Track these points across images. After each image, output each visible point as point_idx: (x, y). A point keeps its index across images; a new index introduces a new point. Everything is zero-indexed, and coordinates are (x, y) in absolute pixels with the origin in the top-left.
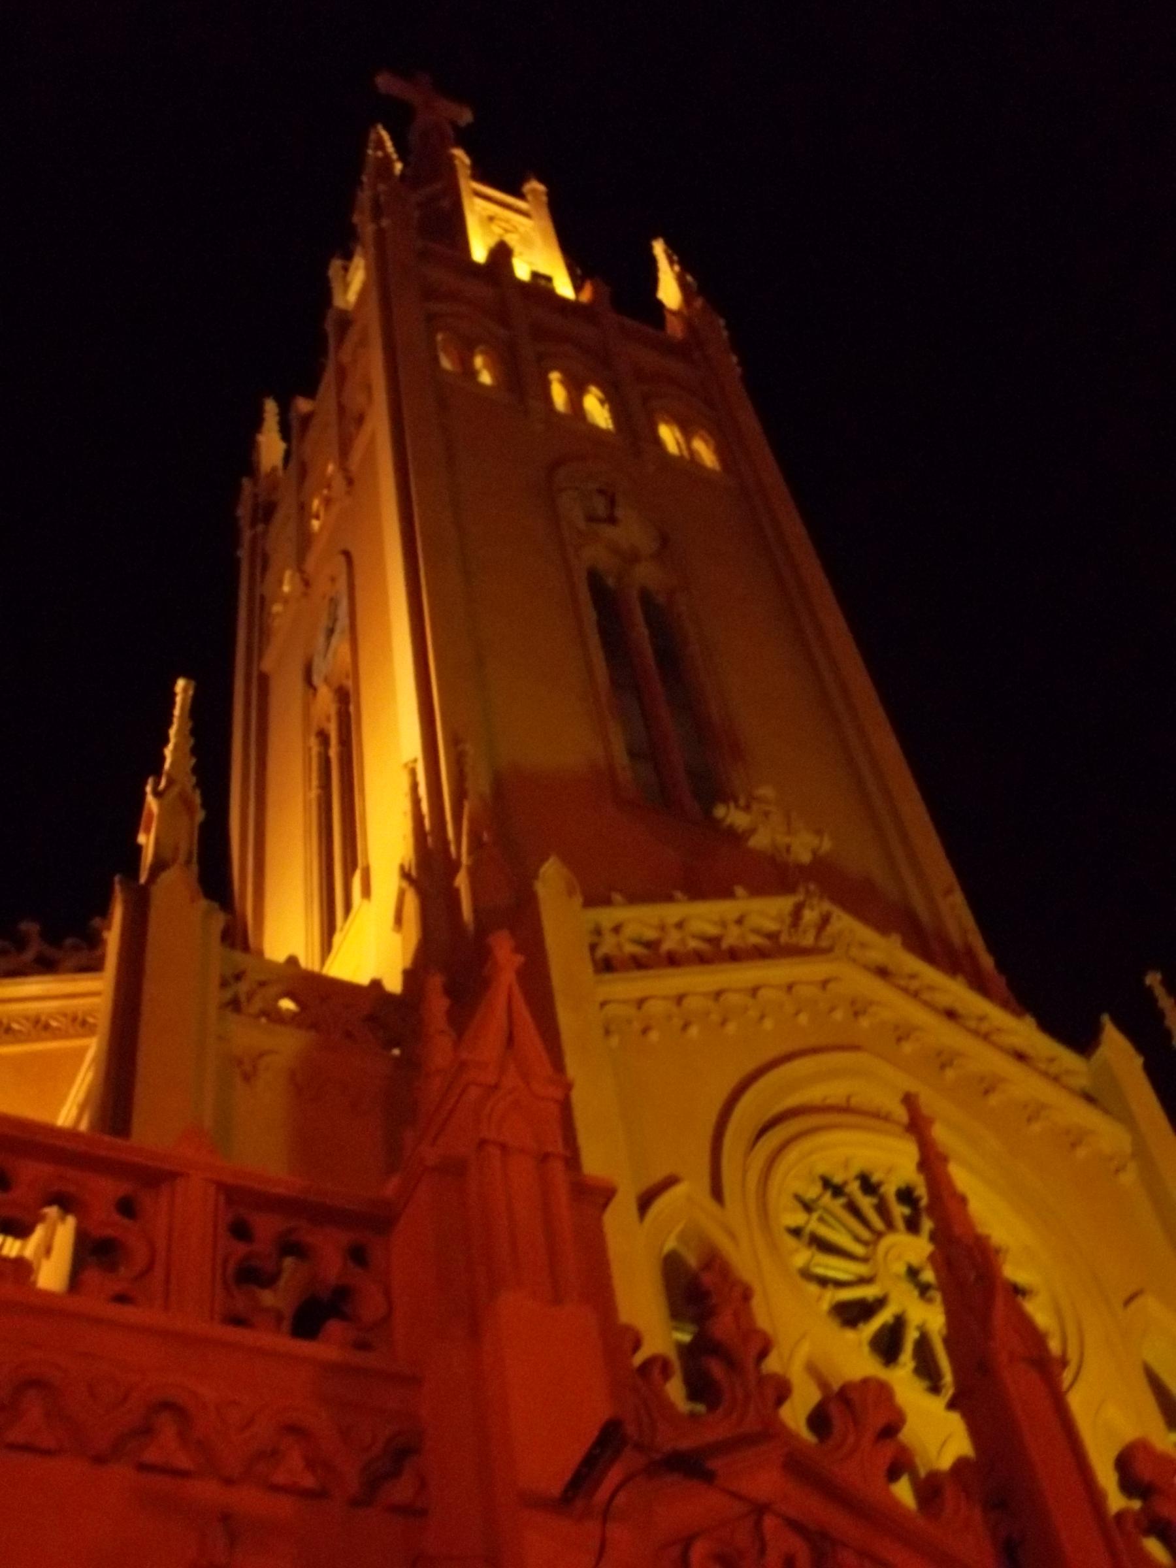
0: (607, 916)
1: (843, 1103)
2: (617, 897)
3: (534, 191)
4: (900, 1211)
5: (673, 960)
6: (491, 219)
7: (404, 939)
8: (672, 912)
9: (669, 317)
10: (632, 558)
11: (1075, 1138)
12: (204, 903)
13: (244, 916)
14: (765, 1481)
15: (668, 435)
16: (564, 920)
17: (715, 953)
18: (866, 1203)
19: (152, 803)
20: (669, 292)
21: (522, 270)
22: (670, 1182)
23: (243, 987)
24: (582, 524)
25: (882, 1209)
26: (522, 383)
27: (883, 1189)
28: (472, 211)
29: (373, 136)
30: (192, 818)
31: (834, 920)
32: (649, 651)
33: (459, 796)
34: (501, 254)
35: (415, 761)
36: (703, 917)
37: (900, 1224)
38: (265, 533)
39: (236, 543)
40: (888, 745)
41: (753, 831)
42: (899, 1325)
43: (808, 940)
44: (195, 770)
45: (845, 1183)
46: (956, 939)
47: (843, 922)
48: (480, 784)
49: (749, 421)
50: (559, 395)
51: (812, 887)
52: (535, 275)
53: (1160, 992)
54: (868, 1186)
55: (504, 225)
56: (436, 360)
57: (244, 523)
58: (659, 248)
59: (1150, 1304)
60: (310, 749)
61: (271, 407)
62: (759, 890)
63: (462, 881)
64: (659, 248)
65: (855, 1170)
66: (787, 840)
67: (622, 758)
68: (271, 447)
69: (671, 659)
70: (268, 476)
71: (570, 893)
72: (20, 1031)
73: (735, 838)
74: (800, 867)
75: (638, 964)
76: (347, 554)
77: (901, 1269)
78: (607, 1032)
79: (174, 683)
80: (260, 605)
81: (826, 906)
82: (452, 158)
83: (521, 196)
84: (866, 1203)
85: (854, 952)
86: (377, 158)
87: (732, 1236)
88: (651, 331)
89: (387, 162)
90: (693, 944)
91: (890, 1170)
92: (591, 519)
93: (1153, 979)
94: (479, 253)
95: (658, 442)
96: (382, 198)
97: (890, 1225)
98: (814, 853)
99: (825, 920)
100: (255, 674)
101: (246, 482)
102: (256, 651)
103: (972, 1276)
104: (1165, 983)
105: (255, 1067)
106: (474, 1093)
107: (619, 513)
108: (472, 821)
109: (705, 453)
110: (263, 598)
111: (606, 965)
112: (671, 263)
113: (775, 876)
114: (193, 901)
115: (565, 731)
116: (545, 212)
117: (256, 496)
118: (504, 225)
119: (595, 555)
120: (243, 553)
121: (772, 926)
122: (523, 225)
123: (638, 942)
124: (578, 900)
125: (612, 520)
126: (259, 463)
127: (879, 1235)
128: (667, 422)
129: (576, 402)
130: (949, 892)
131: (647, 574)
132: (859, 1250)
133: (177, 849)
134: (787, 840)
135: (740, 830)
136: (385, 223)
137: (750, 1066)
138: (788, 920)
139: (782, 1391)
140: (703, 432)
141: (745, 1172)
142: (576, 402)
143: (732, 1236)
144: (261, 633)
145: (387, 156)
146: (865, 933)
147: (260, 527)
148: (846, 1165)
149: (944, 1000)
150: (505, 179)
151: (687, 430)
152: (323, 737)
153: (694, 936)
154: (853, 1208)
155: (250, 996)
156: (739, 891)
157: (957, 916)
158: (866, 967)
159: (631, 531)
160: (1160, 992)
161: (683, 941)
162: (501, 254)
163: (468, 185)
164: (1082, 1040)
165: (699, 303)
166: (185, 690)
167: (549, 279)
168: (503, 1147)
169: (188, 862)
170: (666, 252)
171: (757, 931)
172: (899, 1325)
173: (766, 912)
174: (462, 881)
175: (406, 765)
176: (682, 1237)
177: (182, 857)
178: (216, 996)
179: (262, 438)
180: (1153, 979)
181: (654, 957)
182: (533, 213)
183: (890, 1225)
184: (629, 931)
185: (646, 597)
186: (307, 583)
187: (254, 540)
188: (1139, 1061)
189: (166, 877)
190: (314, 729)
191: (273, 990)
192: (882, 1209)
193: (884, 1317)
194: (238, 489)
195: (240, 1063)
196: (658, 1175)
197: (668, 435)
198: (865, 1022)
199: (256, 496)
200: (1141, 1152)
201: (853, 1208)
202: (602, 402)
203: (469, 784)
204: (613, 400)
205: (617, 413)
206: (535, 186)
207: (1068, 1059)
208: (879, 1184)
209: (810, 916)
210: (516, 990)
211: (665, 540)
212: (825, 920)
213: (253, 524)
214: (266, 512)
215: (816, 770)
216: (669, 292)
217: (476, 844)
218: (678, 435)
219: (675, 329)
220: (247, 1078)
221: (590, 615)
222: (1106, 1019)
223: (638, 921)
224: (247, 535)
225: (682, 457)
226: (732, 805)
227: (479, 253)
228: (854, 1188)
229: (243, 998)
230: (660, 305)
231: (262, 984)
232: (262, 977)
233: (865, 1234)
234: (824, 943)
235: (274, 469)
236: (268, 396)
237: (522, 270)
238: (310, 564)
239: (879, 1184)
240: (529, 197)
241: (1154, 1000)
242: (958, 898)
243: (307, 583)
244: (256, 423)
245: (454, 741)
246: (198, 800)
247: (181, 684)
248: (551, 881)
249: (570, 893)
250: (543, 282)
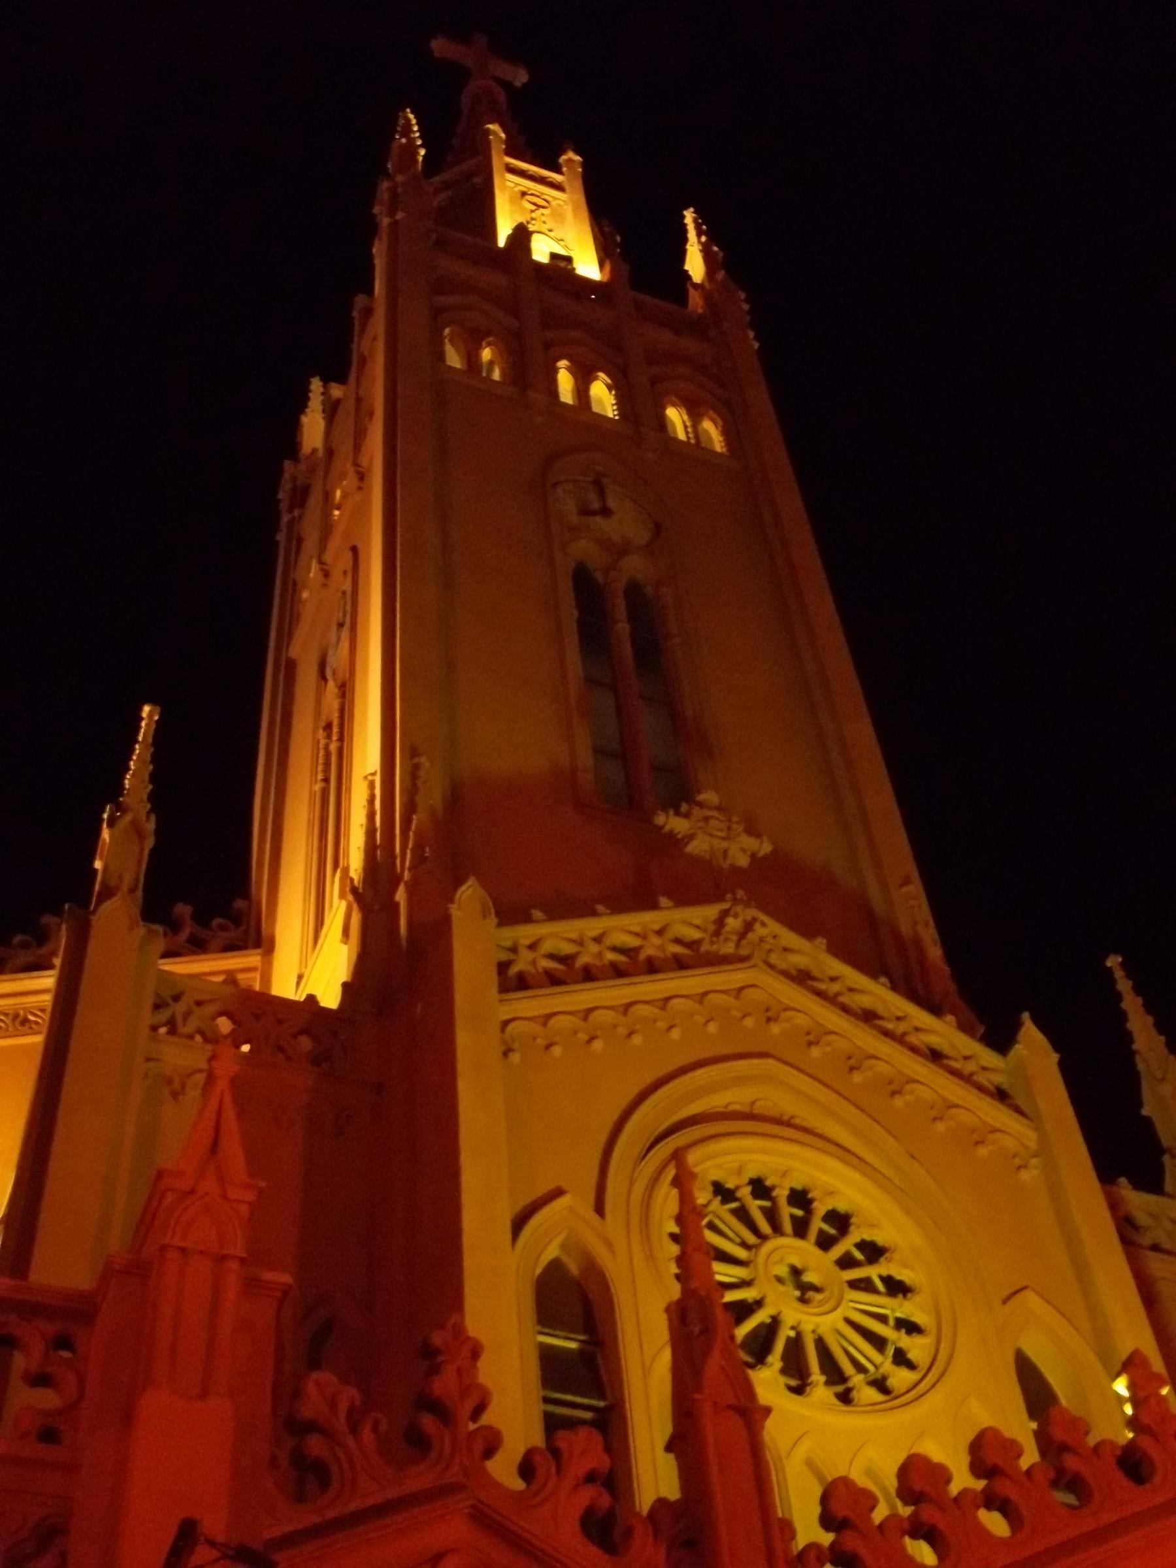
0: (525, 933)
1: (746, 1109)
2: (537, 914)
3: (570, 160)
4: (787, 1212)
5: (589, 975)
6: (524, 194)
7: (349, 950)
8: (590, 926)
9: (692, 291)
10: (623, 550)
11: (980, 1136)
12: (141, 930)
13: (259, 903)
14: (451, 1529)
15: (675, 416)
16: (475, 938)
17: (632, 965)
18: (755, 1206)
19: (106, 834)
20: (695, 265)
21: (541, 250)
22: (558, 1193)
23: (180, 1008)
24: (575, 519)
25: (772, 1215)
26: (530, 375)
27: (774, 1194)
28: (504, 187)
29: (402, 121)
30: (141, 844)
31: (757, 926)
32: (628, 649)
33: (410, 808)
34: (522, 235)
35: (374, 774)
36: (623, 928)
37: (787, 1226)
38: (300, 517)
39: (275, 527)
40: (862, 734)
41: (690, 837)
42: (773, 1326)
43: (729, 948)
44: (152, 797)
45: (738, 1188)
46: (905, 928)
47: (770, 928)
48: (433, 795)
49: (760, 398)
50: (565, 382)
51: (740, 893)
52: (554, 256)
53: (1119, 974)
54: (760, 1188)
55: (535, 200)
56: (441, 356)
57: (283, 506)
58: (689, 216)
59: (1032, 1301)
60: (318, 741)
61: (316, 385)
62: (684, 899)
63: (401, 895)
64: (689, 216)
65: (752, 1173)
66: (725, 845)
67: (585, 758)
68: (313, 428)
69: (650, 650)
70: (308, 457)
71: (485, 916)
72: (37, 1023)
73: (674, 842)
74: (735, 870)
75: (553, 980)
76: (354, 550)
77: (783, 1271)
78: (775, 937)
79: (140, 710)
80: (292, 589)
81: (752, 913)
82: (488, 132)
83: (557, 169)
84: (755, 1206)
85: (774, 958)
86: (402, 145)
87: (609, 1245)
88: (676, 307)
89: (412, 150)
90: (611, 956)
91: (784, 1174)
92: (585, 512)
93: (1113, 961)
94: (503, 232)
95: (662, 424)
96: (400, 190)
97: (777, 1229)
98: (753, 856)
99: (749, 926)
100: (284, 659)
101: (288, 464)
102: (286, 637)
103: (697, 1330)
104: (1123, 965)
105: (183, 1087)
106: (169, 1198)
107: (612, 503)
108: (418, 834)
109: (712, 432)
110: (295, 583)
111: (522, 983)
112: (699, 234)
113: (699, 883)
114: (131, 929)
115: (529, 733)
116: (578, 184)
117: (294, 479)
118: (535, 200)
119: (584, 549)
120: (281, 537)
121: (695, 935)
122: (555, 199)
123: (552, 957)
124: (493, 920)
125: (606, 512)
126: (301, 443)
127: (763, 1237)
128: (674, 405)
129: (582, 391)
130: (906, 881)
131: (635, 566)
132: (741, 1253)
133: (120, 877)
134: (725, 845)
135: (679, 836)
136: (399, 216)
137: (649, 1079)
138: (712, 928)
139: (492, 1444)
140: (711, 413)
141: (632, 1182)
142: (582, 391)
143: (609, 1245)
144: (291, 618)
145: (411, 141)
146: (790, 938)
147: (296, 513)
148: (739, 1171)
149: (863, 1001)
150: (539, 150)
151: (695, 412)
152: (328, 727)
153: (614, 949)
154: (742, 1214)
155: (187, 1015)
156: (664, 901)
157: (910, 909)
158: (786, 974)
159: (626, 522)
160: (1119, 974)
161: (600, 955)
162: (522, 235)
163: (500, 159)
164: (1000, 1039)
165: (721, 275)
166: (150, 715)
167: (569, 260)
168: (183, 1251)
169: (132, 891)
170: (695, 221)
171: (677, 941)
172: (773, 1326)
173: (689, 922)
174: (401, 895)
175: (366, 777)
176: (563, 1247)
177: (125, 888)
178: (147, 1017)
179: (305, 420)
180: (1113, 961)
181: (567, 972)
182: (567, 187)
183: (777, 1229)
184: (547, 947)
185: (633, 590)
186: (327, 575)
187: (291, 524)
188: (1055, 1057)
189: (108, 906)
190: (323, 724)
191: (209, 1009)
192: (772, 1215)
193: (760, 1317)
194: (280, 472)
195: (170, 1081)
196: (541, 1190)
197: (675, 416)
198: (775, 1029)
199: (294, 479)
200: (1044, 1150)
201: (742, 1214)
202: (609, 388)
203: (420, 799)
204: (619, 387)
205: (622, 402)
206: (571, 156)
207: (988, 1057)
208: (772, 1188)
209: (733, 923)
210: (228, 1099)
211: (658, 529)
212: (749, 926)
213: (290, 510)
214: (301, 496)
215: (792, 755)
216: (695, 265)
217: (419, 859)
218: (686, 417)
219: (696, 301)
220: (175, 1095)
221: (570, 614)
222: (1026, 1016)
223: (556, 935)
224: (285, 518)
225: (688, 443)
226: (671, 812)
227: (503, 232)
228: (745, 1192)
229: (179, 1019)
230: (686, 276)
231: (199, 1004)
232: (199, 997)
233: (751, 1239)
234: (744, 952)
235: (315, 451)
236: (313, 376)
237: (541, 250)
238: (328, 557)
239: (772, 1188)
240: (564, 169)
241: (1113, 982)
242: (916, 888)
243: (327, 575)
244: (301, 404)
245: (412, 752)
246: (151, 826)
247: (147, 709)
248: (468, 903)
249: (485, 916)
250: (563, 264)
